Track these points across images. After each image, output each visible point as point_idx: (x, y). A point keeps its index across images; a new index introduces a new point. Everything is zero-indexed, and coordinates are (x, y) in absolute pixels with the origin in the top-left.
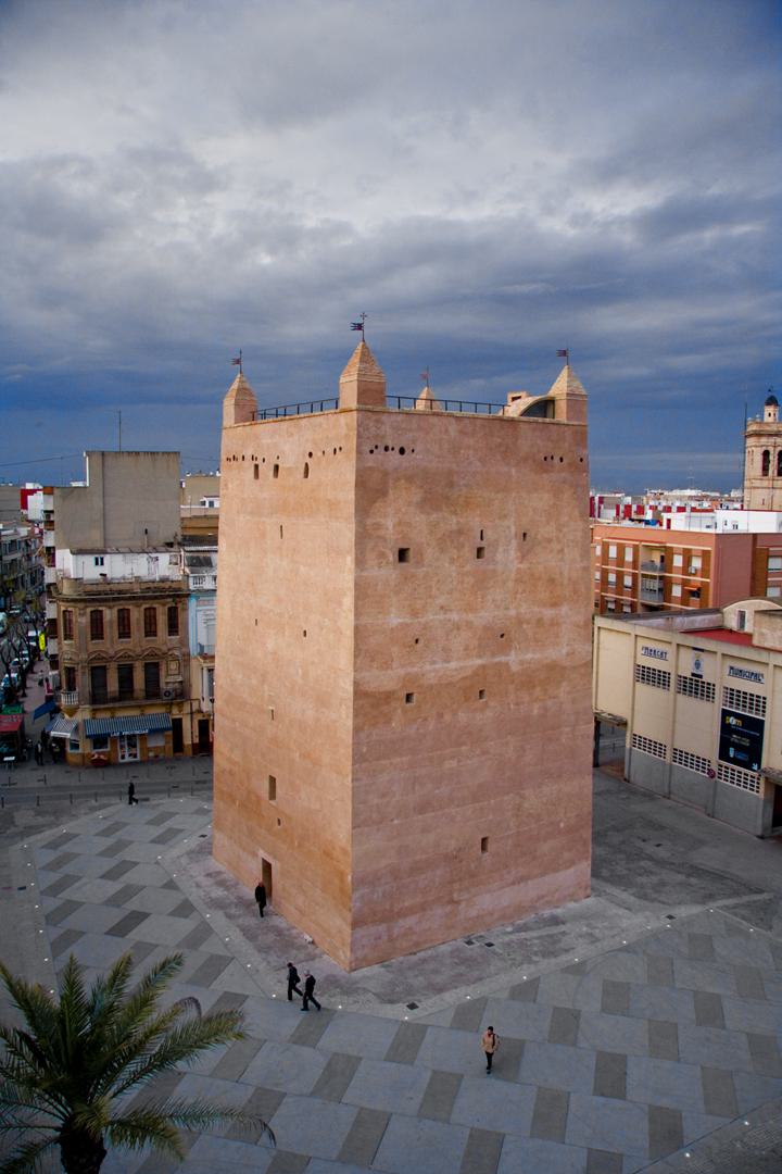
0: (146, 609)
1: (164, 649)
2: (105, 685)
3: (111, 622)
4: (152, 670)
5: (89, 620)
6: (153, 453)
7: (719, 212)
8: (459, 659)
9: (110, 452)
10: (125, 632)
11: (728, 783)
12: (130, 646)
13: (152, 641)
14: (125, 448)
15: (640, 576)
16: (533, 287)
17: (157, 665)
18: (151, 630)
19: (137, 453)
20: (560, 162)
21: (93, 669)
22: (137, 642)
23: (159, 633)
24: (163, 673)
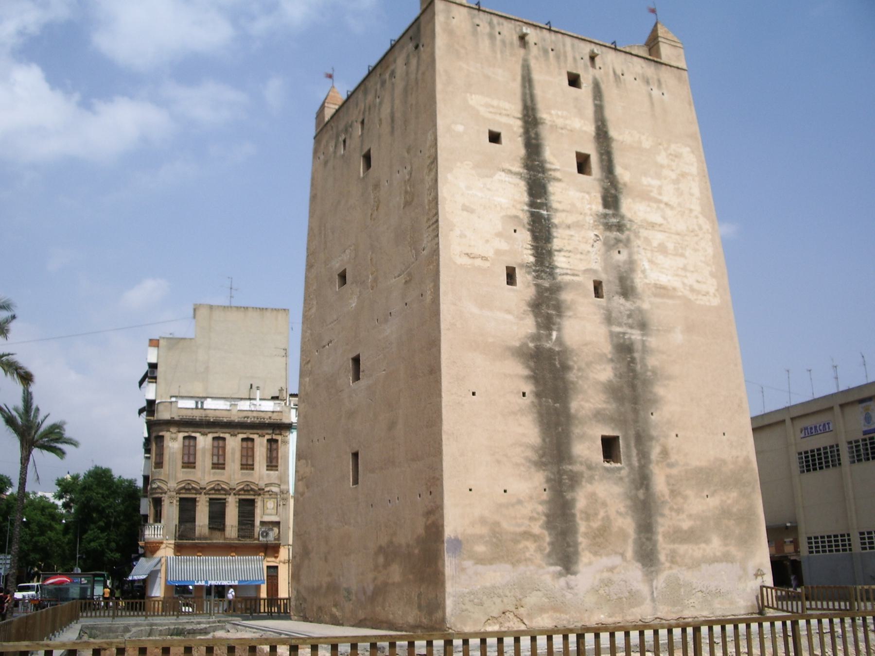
0: (243, 440)
1: (262, 484)
2: (193, 520)
3: (204, 448)
4: (247, 508)
5: (181, 446)
6: (262, 309)
7: (35, 433)
8: (145, 636)
9: (215, 306)
10: (219, 465)
11: (868, 550)
12: (223, 478)
13: (249, 475)
14: (235, 303)
15: (271, 561)
16: (32, 415)
17: (252, 502)
18: (247, 465)
19: (246, 308)
20: (530, 243)
21: (181, 500)
22: (233, 475)
23: (257, 466)
24: (258, 511)
